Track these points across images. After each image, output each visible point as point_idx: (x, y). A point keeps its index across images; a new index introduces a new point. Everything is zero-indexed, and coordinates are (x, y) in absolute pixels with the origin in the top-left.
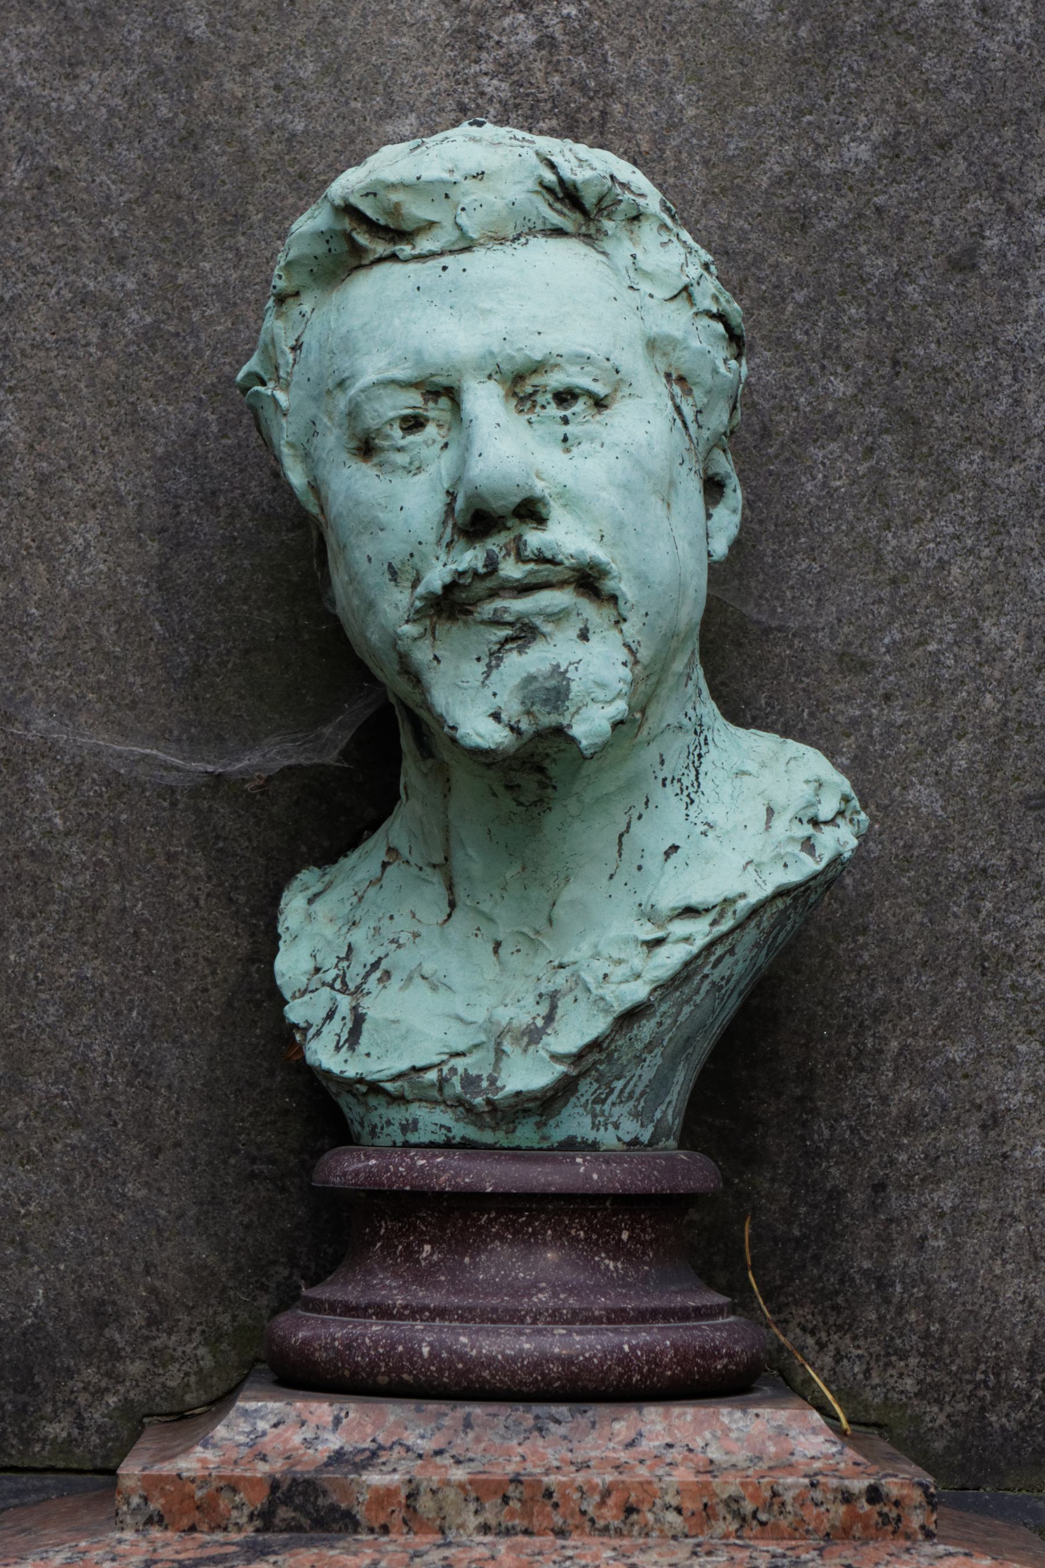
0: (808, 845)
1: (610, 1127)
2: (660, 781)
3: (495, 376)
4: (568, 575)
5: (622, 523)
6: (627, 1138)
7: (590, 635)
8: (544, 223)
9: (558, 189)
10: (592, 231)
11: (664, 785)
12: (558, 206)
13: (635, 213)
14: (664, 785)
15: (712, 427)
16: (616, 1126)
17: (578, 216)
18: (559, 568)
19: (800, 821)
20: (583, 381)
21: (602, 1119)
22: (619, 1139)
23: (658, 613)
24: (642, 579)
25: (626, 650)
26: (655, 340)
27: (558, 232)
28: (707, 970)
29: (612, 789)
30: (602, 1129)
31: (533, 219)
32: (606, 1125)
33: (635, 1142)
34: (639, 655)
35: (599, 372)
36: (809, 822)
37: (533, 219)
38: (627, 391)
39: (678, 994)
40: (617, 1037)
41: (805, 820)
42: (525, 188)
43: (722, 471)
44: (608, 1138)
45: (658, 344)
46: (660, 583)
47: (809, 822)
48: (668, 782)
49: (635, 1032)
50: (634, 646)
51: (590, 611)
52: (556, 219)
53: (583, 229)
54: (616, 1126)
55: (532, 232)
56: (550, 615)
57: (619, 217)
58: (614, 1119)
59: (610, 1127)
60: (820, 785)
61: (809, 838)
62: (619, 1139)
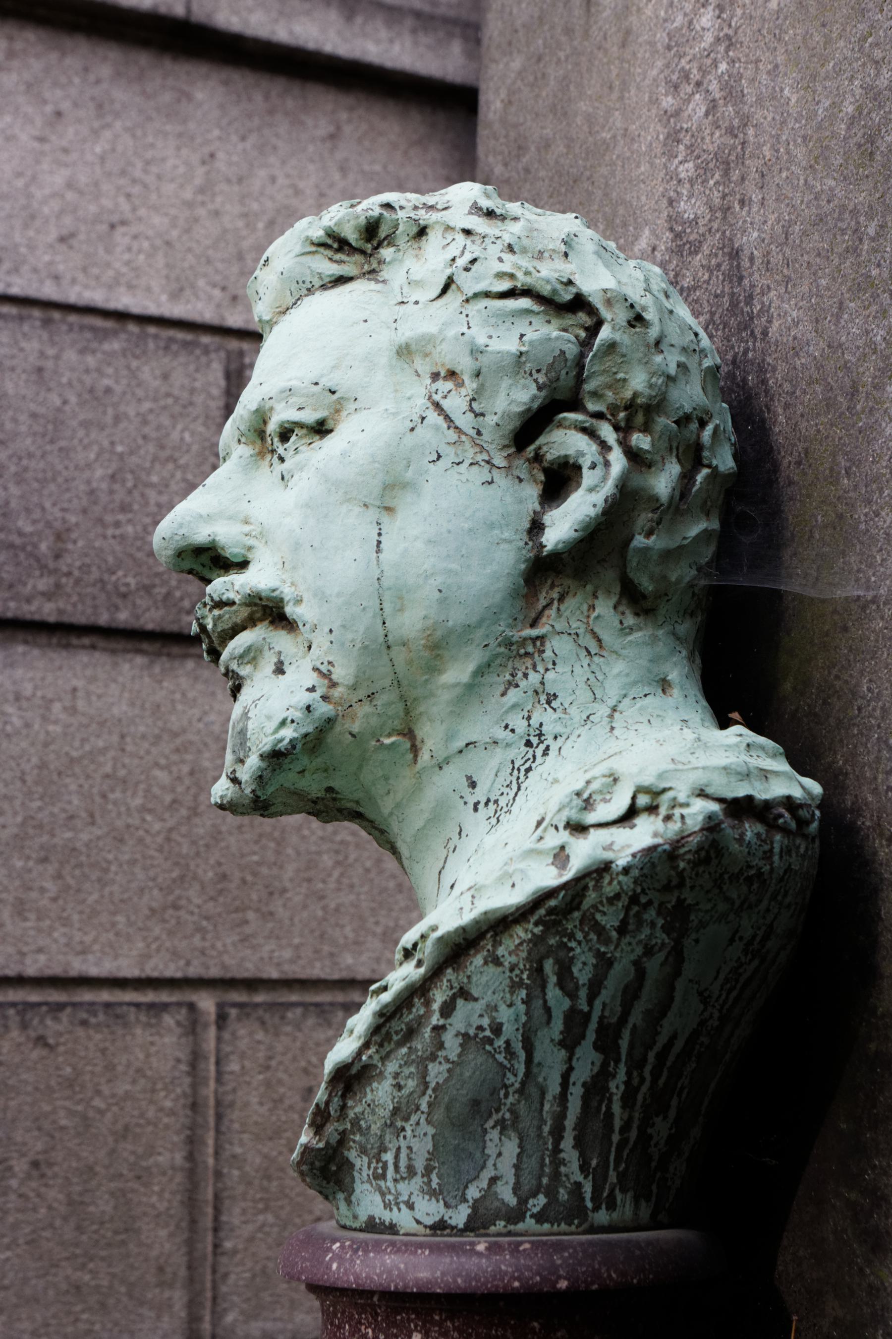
0: (561, 856)
1: (402, 1206)
2: (471, 806)
3: (243, 440)
4: (245, 612)
5: (297, 543)
6: (429, 1221)
7: (286, 668)
8: (321, 278)
9: (330, 242)
10: (375, 265)
11: (476, 809)
12: (338, 256)
13: (415, 230)
14: (476, 809)
15: (499, 411)
16: (411, 1206)
17: (358, 258)
18: (234, 608)
19: (556, 828)
20: (293, 415)
21: (391, 1197)
22: (418, 1222)
23: (344, 626)
24: (322, 597)
25: (315, 674)
26: (408, 346)
27: (341, 280)
28: (435, 1019)
29: (420, 824)
30: (395, 1209)
31: (308, 280)
32: (397, 1204)
33: (440, 1226)
34: (334, 677)
35: (303, 399)
36: (565, 828)
37: (308, 280)
38: (352, 406)
39: (404, 1050)
40: (350, 1103)
41: (561, 826)
42: (293, 254)
43: (571, 452)
44: (404, 1219)
45: (413, 347)
46: (339, 595)
47: (565, 828)
48: (481, 806)
49: (369, 1096)
50: (324, 669)
51: (281, 640)
52: (334, 270)
53: (366, 267)
54: (411, 1206)
55: (310, 291)
56: (241, 657)
57: (402, 241)
58: (406, 1198)
59: (402, 1206)
60: (615, 780)
61: (563, 848)
62: (418, 1222)
